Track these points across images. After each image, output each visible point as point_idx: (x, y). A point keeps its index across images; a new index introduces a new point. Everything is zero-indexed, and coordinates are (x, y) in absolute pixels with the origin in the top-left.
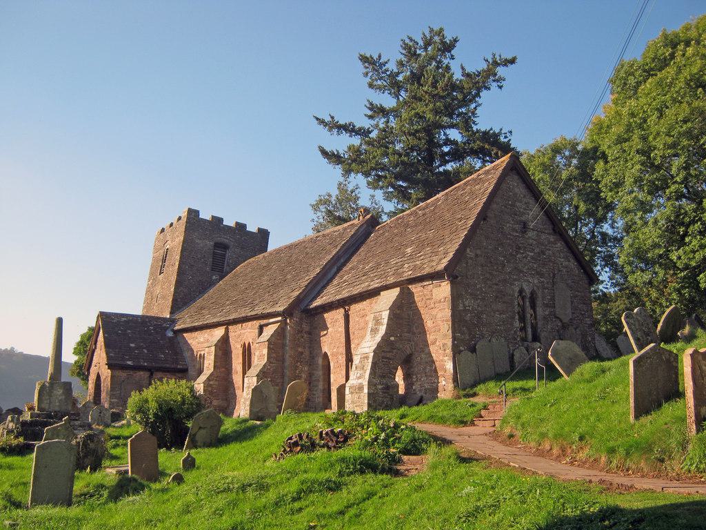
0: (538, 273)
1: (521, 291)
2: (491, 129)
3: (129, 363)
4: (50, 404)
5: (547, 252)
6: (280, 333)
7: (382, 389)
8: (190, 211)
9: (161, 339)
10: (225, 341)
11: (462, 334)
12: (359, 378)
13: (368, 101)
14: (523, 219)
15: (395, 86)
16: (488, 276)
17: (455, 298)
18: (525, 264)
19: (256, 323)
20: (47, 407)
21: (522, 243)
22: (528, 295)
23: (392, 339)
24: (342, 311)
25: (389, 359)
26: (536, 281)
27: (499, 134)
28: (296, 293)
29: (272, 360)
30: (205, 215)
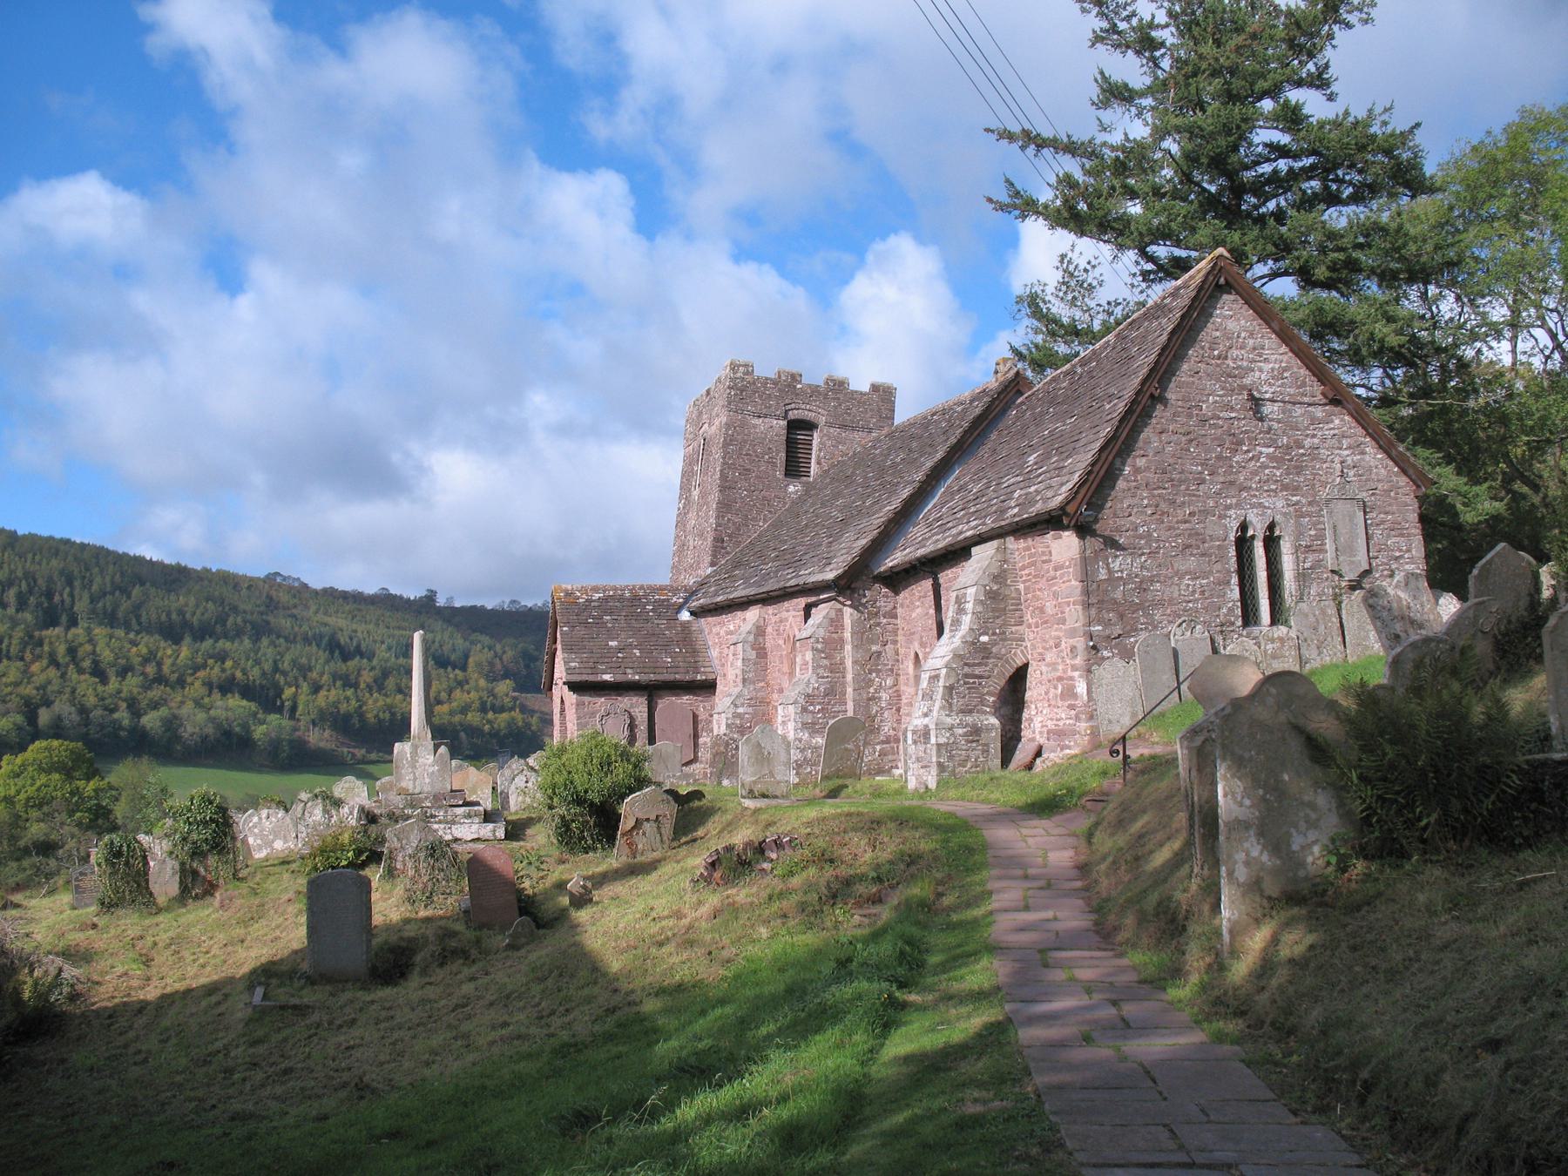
0: (1285, 487)
1: (1244, 527)
2: (1347, 113)
3: (607, 677)
4: (415, 779)
5: (1308, 442)
6: (835, 623)
7: (965, 735)
8: (734, 367)
9: (668, 628)
10: (760, 631)
11: (1107, 624)
12: (926, 715)
13: (1102, 73)
14: (1247, 381)
15: (1145, 43)
16: (1163, 506)
17: (1086, 567)
18: (1255, 473)
19: (802, 602)
20: (411, 787)
21: (1246, 432)
22: (1260, 535)
23: (984, 639)
24: (927, 584)
25: (980, 677)
26: (1280, 504)
27: (1367, 124)
28: (863, 542)
29: (821, 671)
30: (765, 369)
